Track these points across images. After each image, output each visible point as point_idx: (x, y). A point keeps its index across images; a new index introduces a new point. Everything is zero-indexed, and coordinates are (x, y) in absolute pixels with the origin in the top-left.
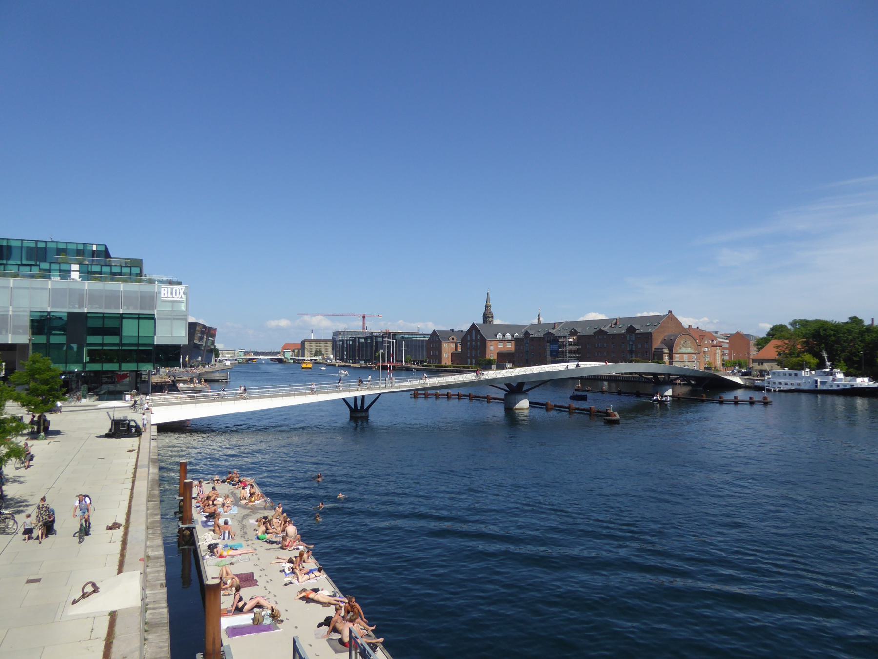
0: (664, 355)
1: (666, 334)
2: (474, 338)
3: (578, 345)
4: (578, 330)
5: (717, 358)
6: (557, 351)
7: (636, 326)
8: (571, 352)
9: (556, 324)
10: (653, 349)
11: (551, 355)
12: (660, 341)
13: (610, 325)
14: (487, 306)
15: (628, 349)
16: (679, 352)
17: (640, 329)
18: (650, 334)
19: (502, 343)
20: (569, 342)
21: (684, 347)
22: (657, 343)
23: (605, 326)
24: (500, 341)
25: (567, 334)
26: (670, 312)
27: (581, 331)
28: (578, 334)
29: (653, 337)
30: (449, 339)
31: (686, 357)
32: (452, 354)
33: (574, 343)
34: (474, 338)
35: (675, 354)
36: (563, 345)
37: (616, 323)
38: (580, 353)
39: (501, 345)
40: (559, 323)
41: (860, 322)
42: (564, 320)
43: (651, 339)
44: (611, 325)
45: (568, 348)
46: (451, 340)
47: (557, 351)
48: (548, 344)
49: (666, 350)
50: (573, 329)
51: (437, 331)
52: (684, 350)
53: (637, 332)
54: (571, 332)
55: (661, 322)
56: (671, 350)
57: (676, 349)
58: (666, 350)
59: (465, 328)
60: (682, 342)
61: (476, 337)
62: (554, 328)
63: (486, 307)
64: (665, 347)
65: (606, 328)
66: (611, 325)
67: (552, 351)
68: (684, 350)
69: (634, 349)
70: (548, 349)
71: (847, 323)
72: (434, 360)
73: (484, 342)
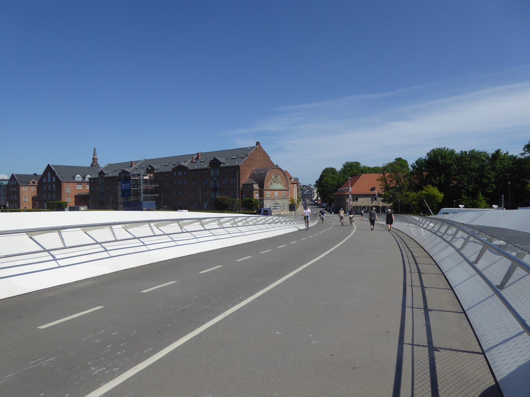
0: (255, 192)
1: (254, 168)
2: (49, 181)
3: (155, 184)
4: (155, 167)
5: (295, 196)
6: (129, 191)
7: (221, 160)
8: (146, 191)
9: (133, 163)
10: (241, 186)
11: (123, 196)
12: (248, 175)
13: (191, 160)
14: (94, 159)
15: (212, 186)
16: (270, 188)
17: (225, 162)
18: (238, 167)
19: (82, 185)
20: (144, 180)
21: (274, 182)
22: (245, 179)
23: (185, 162)
24: (79, 183)
25: (142, 172)
26: (258, 143)
27: (158, 168)
28: (156, 171)
29: (241, 171)
30: (29, 183)
31: (276, 193)
32: (32, 198)
33: (151, 181)
34: (49, 181)
35: (265, 190)
36: (137, 183)
37: (197, 158)
38: (158, 193)
39: (79, 187)
40: (136, 162)
41: (454, 151)
42: (142, 159)
43: (239, 173)
44: (192, 160)
45: (142, 187)
46: (31, 184)
47: (129, 191)
48: (120, 183)
49: (256, 186)
50: (150, 166)
51: (16, 175)
52: (275, 186)
53: (222, 165)
54: (147, 169)
55: (249, 154)
56: (262, 186)
57: (268, 185)
58: (256, 186)
59: (40, 172)
60: (273, 177)
61: (52, 179)
62: (131, 166)
63: (93, 159)
64: (254, 182)
65: (187, 163)
66: (192, 160)
67: (124, 191)
68: (275, 186)
69: (218, 186)
70: (119, 188)
71: (394, 162)
72: (13, 205)
73: (59, 184)
